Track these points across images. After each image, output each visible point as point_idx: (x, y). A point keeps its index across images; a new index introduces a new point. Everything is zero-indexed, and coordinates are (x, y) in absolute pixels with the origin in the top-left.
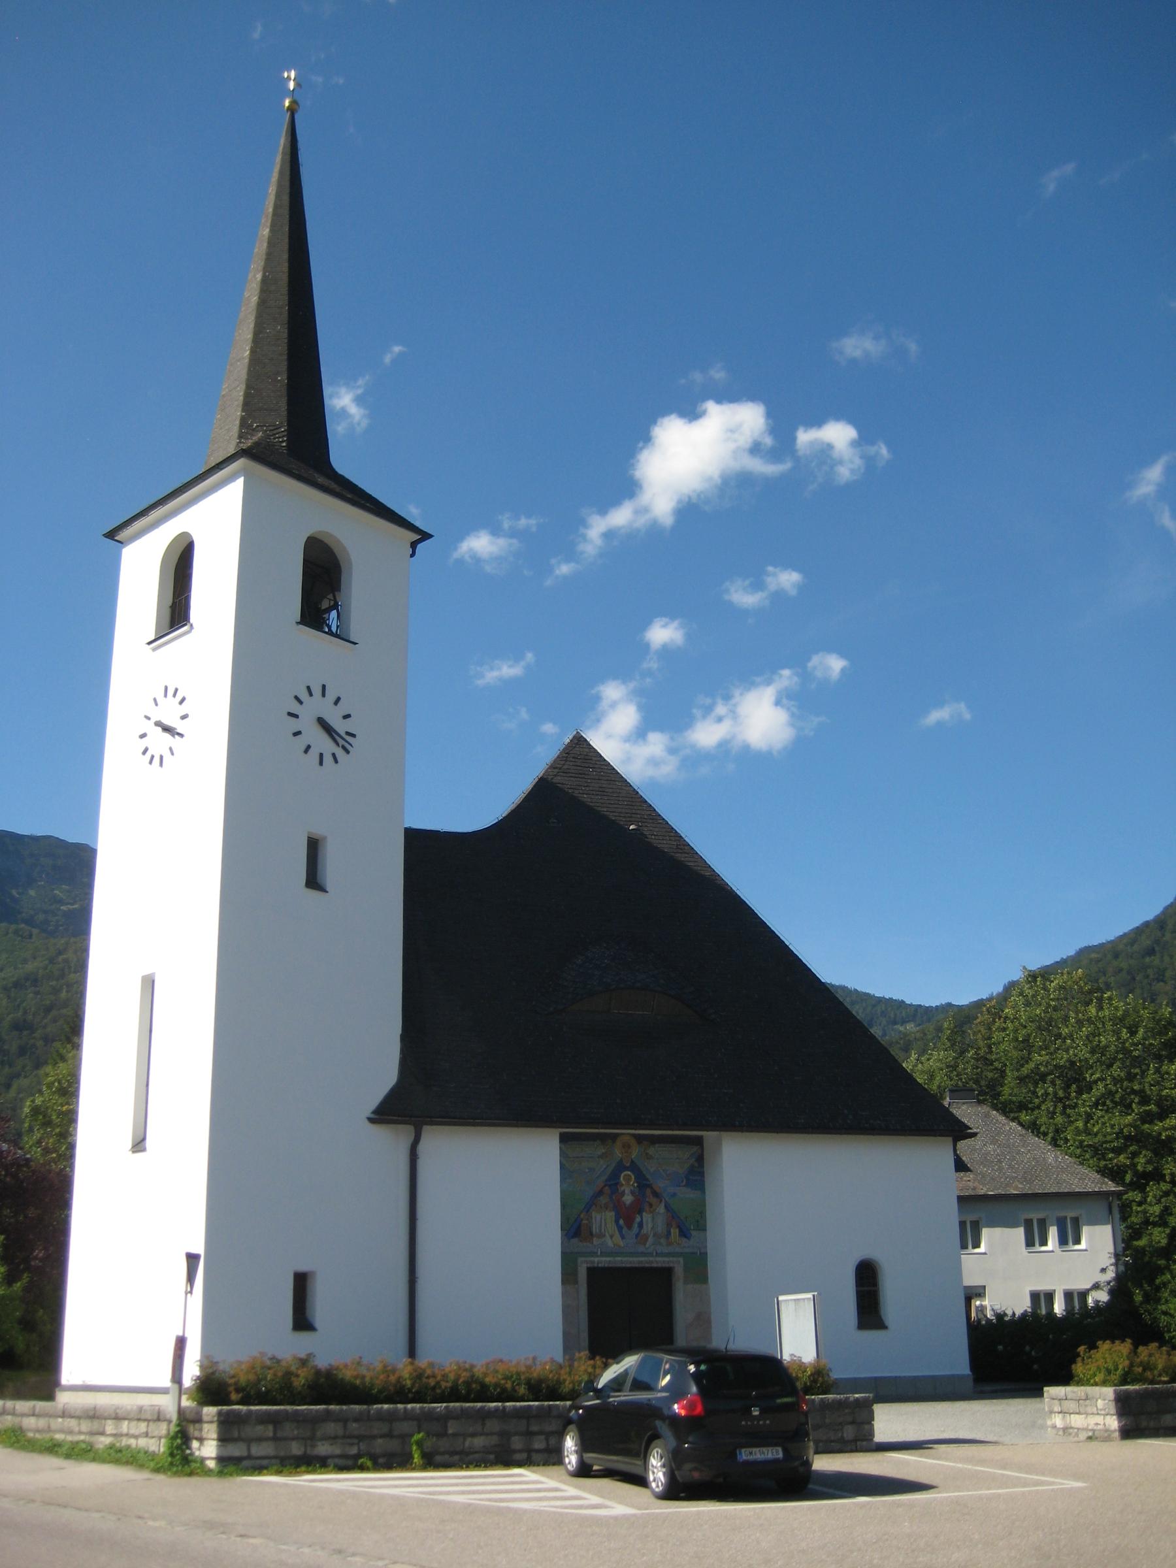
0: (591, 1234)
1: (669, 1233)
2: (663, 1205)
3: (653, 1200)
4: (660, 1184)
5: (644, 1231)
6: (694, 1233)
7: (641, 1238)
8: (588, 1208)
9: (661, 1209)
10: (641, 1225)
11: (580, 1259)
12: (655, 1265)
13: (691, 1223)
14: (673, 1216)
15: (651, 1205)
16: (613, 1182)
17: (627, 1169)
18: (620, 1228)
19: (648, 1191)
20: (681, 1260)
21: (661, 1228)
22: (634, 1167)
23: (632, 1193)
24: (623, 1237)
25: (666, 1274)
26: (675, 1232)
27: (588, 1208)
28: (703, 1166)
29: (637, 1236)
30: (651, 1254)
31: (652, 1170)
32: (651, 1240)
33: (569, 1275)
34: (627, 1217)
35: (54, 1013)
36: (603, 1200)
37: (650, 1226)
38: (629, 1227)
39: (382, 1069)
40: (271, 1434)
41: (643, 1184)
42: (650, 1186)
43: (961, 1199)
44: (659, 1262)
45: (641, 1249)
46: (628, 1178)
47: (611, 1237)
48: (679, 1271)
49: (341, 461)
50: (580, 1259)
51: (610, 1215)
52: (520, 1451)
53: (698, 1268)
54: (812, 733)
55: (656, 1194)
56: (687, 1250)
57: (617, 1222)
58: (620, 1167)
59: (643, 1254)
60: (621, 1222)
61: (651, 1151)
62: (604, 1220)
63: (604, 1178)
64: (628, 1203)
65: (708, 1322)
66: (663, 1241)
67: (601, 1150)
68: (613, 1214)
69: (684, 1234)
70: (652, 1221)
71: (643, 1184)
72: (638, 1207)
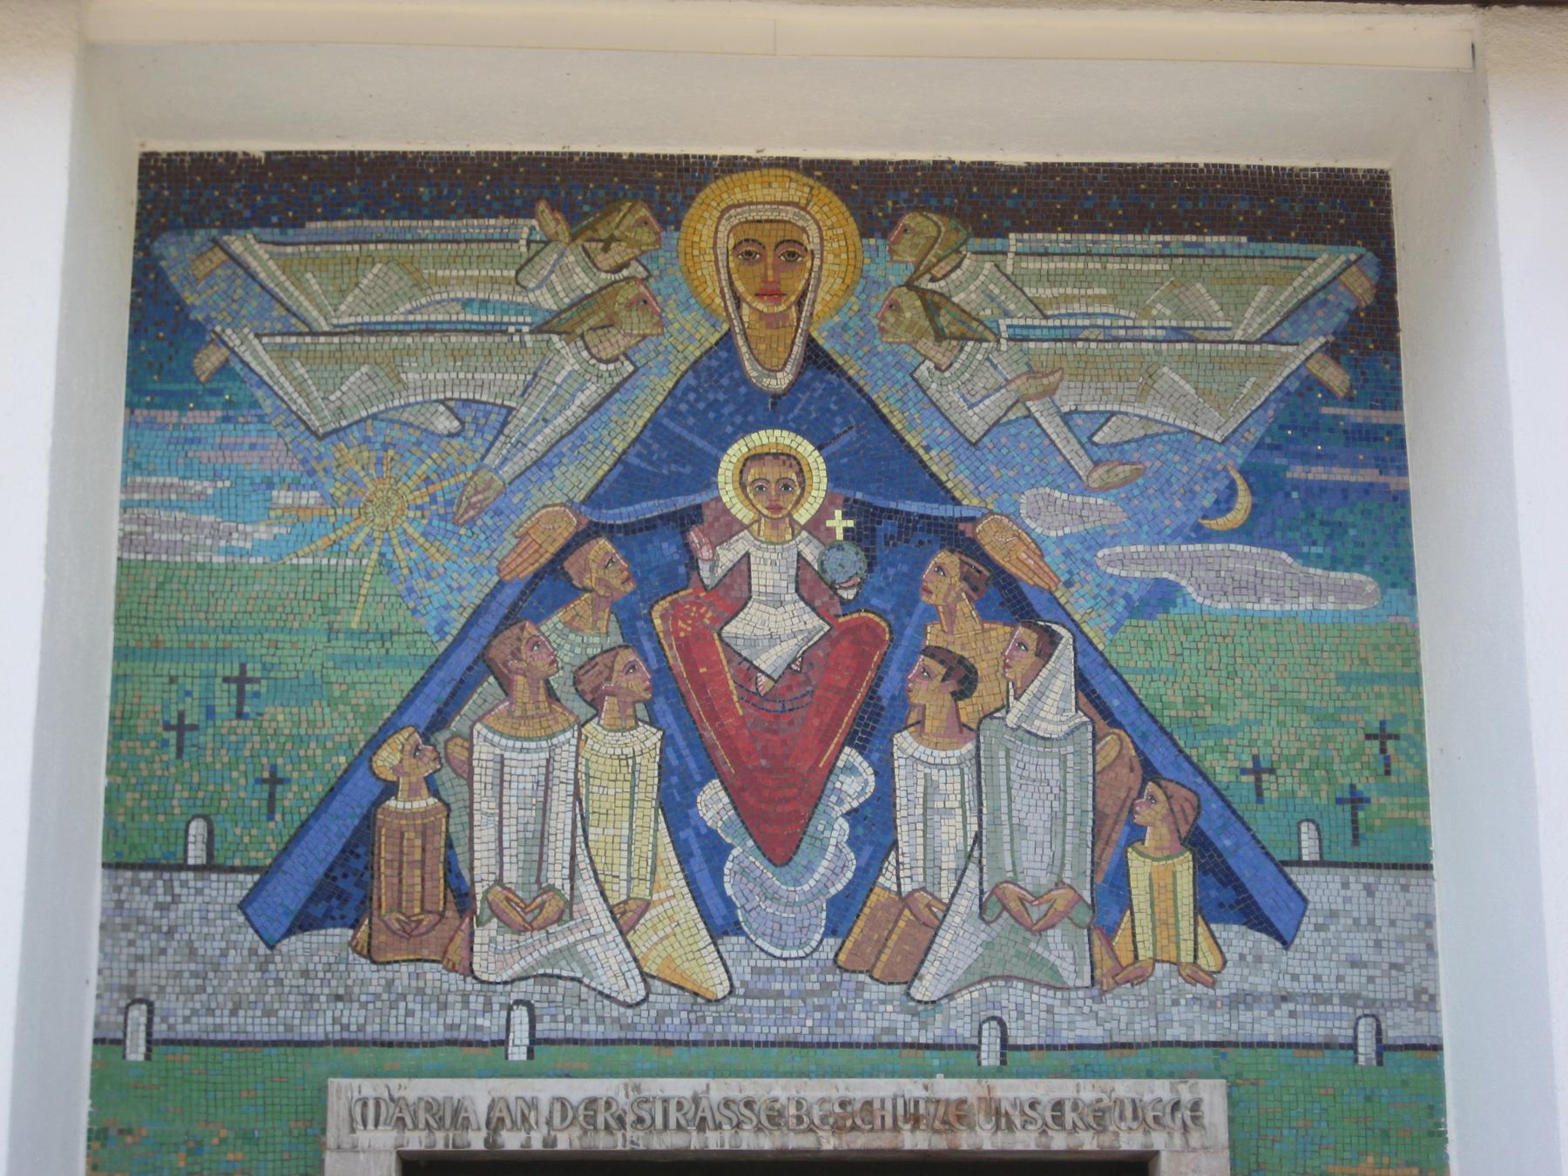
0: (461, 897)
1: (1113, 890)
2: (1060, 675)
4: (1036, 524)
5: (903, 873)
6: (1320, 887)
9: (1052, 701)
10: (875, 826)
11: (344, 1092)
12: (983, 1139)
15: (964, 679)
16: (653, 508)
17: (774, 410)
18: (702, 856)
19: (943, 575)
20: (1212, 1095)
21: (1043, 838)
22: (825, 394)
23: (810, 585)
24: (722, 923)
26: (1162, 877)
27: (436, 709)
28: (1388, 393)
29: (842, 912)
30: (956, 1054)
31: (974, 422)
32: (958, 945)
34: (755, 765)
35: (952, 1119)
36: (571, 638)
37: (952, 834)
38: (781, 841)
41: (897, 514)
42: (953, 534)
43: (1427, 867)
45: (876, 1011)
46: (776, 484)
47: (626, 918)
50: (344, 1092)
51: (625, 750)
54: (908, 220)
55: (1006, 598)
56: (1268, 1025)
57: (675, 805)
58: (718, 397)
59: (888, 1052)
60: (713, 804)
61: (972, 281)
63: (579, 477)
64: (771, 660)
66: (1062, 950)
67: (567, 276)
68: (648, 739)
70: (985, 791)
71: (897, 514)
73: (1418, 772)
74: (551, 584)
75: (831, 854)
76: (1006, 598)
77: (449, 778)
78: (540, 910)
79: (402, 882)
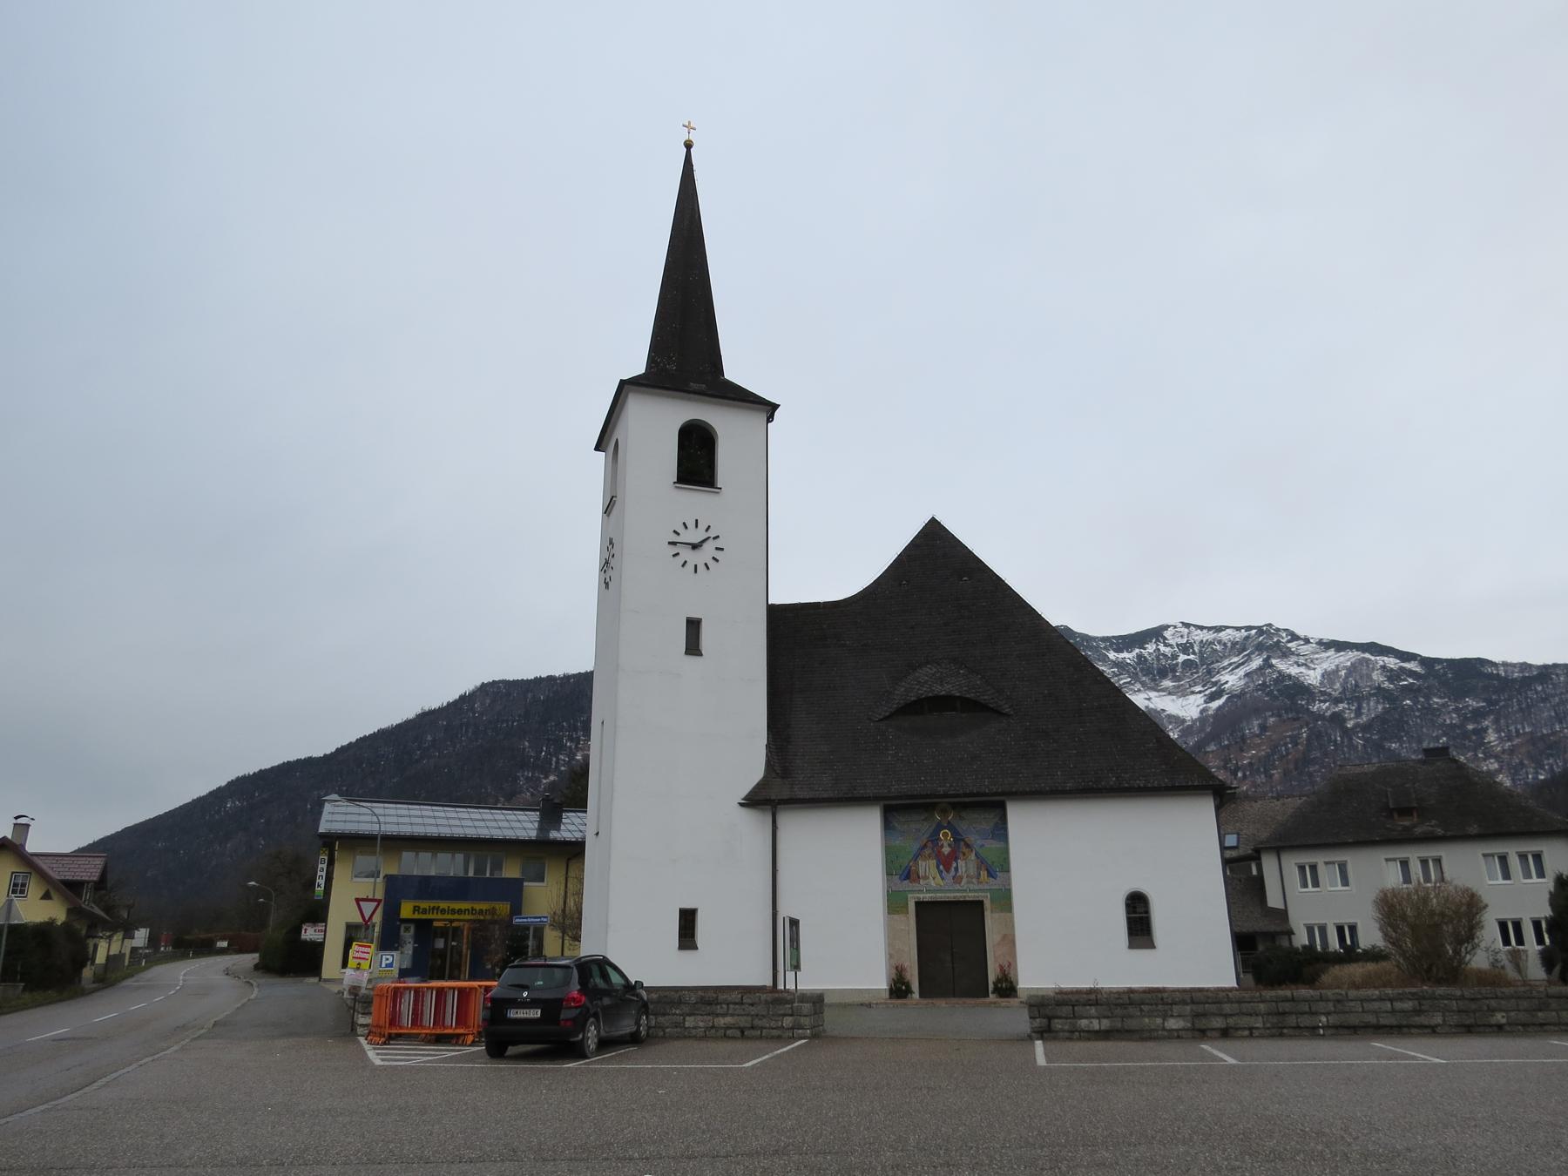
3: (965, 850)
7: (957, 879)
8: (916, 858)
9: (973, 856)
10: (956, 869)
13: (998, 867)
14: (982, 863)
16: (934, 839)
18: (940, 872)
21: (973, 871)
22: (950, 826)
25: (979, 905)
26: (984, 874)
27: (916, 858)
33: (894, 904)
34: (946, 863)
36: (927, 852)
38: (948, 870)
39: (752, 767)
40: (1197, 951)
44: (971, 896)
46: (945, 835)
48: (987, 904)
49: (733, 372)
52: (638, 1024)
53: (1004, 901)
55: (968, 846)
62: (927, 867)
65: (1013, 942)
69: (990, 875)
70: (965, 866)
71: (958, 839)
72: (954, 856)
73: (700, 1032)
74: (925, 846)
75: (953, 872)
76: (968, 846)
77: (917, 864)
78: (926, 878)
79: (913, 876)
